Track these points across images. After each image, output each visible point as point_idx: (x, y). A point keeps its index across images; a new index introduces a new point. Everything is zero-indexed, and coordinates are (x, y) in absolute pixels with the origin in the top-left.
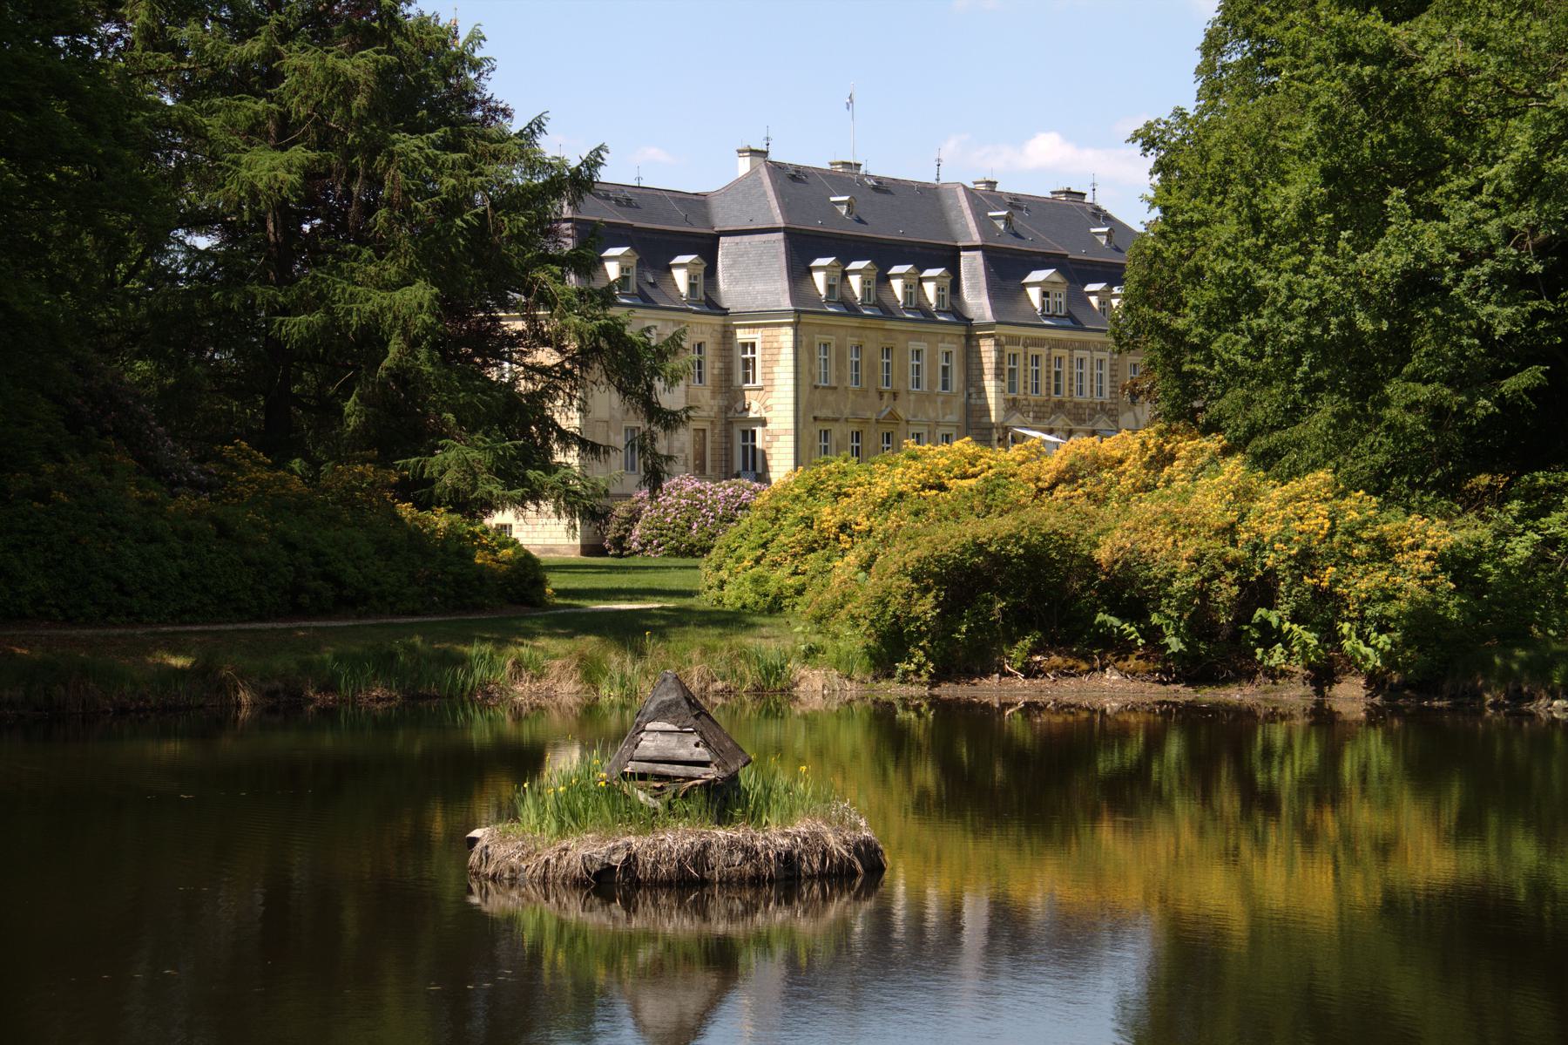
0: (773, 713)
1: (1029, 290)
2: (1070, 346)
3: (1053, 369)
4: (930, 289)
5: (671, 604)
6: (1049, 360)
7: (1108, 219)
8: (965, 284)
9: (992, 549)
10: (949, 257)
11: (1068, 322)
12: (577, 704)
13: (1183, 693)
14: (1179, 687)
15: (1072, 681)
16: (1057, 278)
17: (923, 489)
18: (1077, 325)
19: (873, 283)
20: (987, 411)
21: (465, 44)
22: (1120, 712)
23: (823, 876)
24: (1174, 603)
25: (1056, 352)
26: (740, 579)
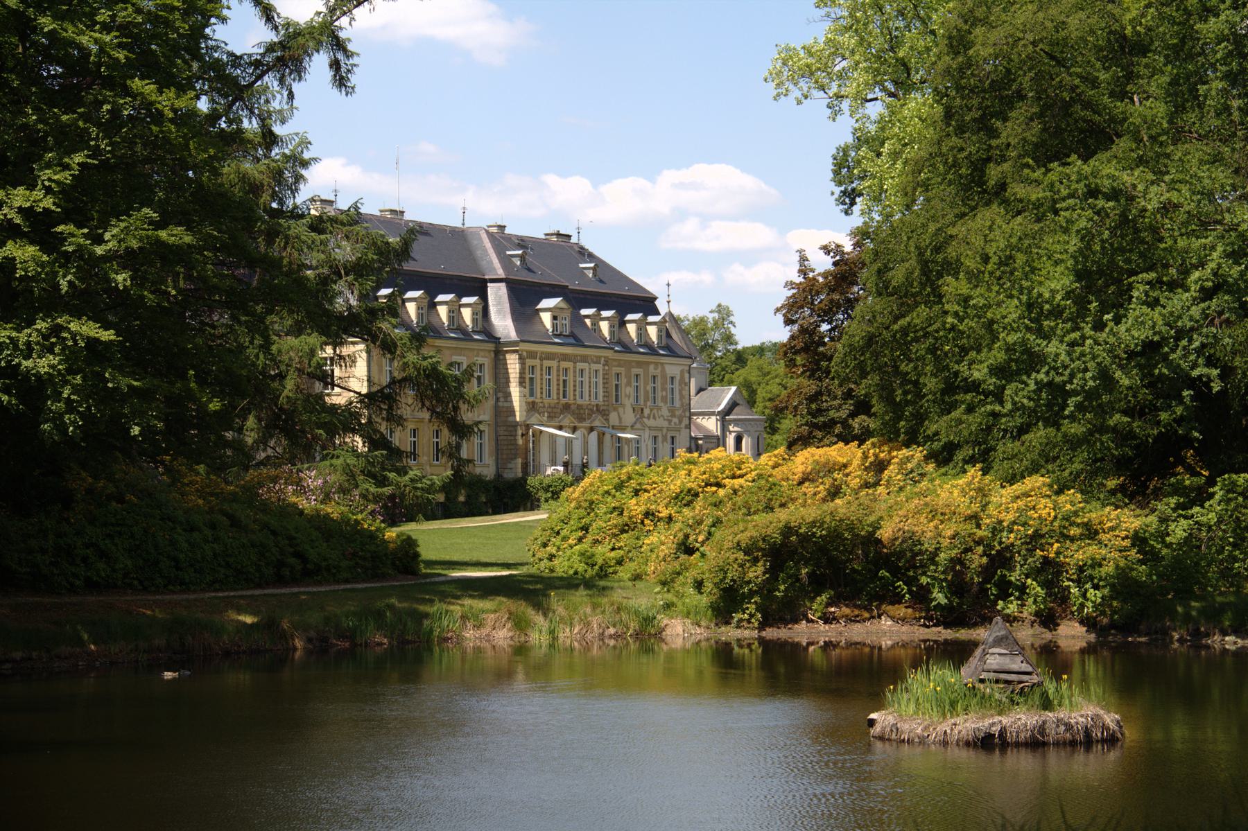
0: (647, 650)
1: (542, 315)
2: (574, 359)
3: (562, 378)
4: (467, 314)
5: (505, 573)
6: (558, 371)
7: (591, 257)
8: (492, 310)
9: (802, 531)
10: (479, 287)
11: (572, 341)
12: (510, 646)
13: (947, 634)
14: (939, 629)
15: (859, 625)
16: (563, 305)
17: (706, 485)
18: (579, 343)
19: (425, 309)
20: (513, 412)
21: (296, 148)
22: (893, 646)
23: (1103, 741)
24: (940, 568)
25: (564, 364)
26: (568, 552)
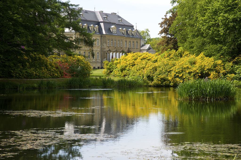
16: (115, 27)
